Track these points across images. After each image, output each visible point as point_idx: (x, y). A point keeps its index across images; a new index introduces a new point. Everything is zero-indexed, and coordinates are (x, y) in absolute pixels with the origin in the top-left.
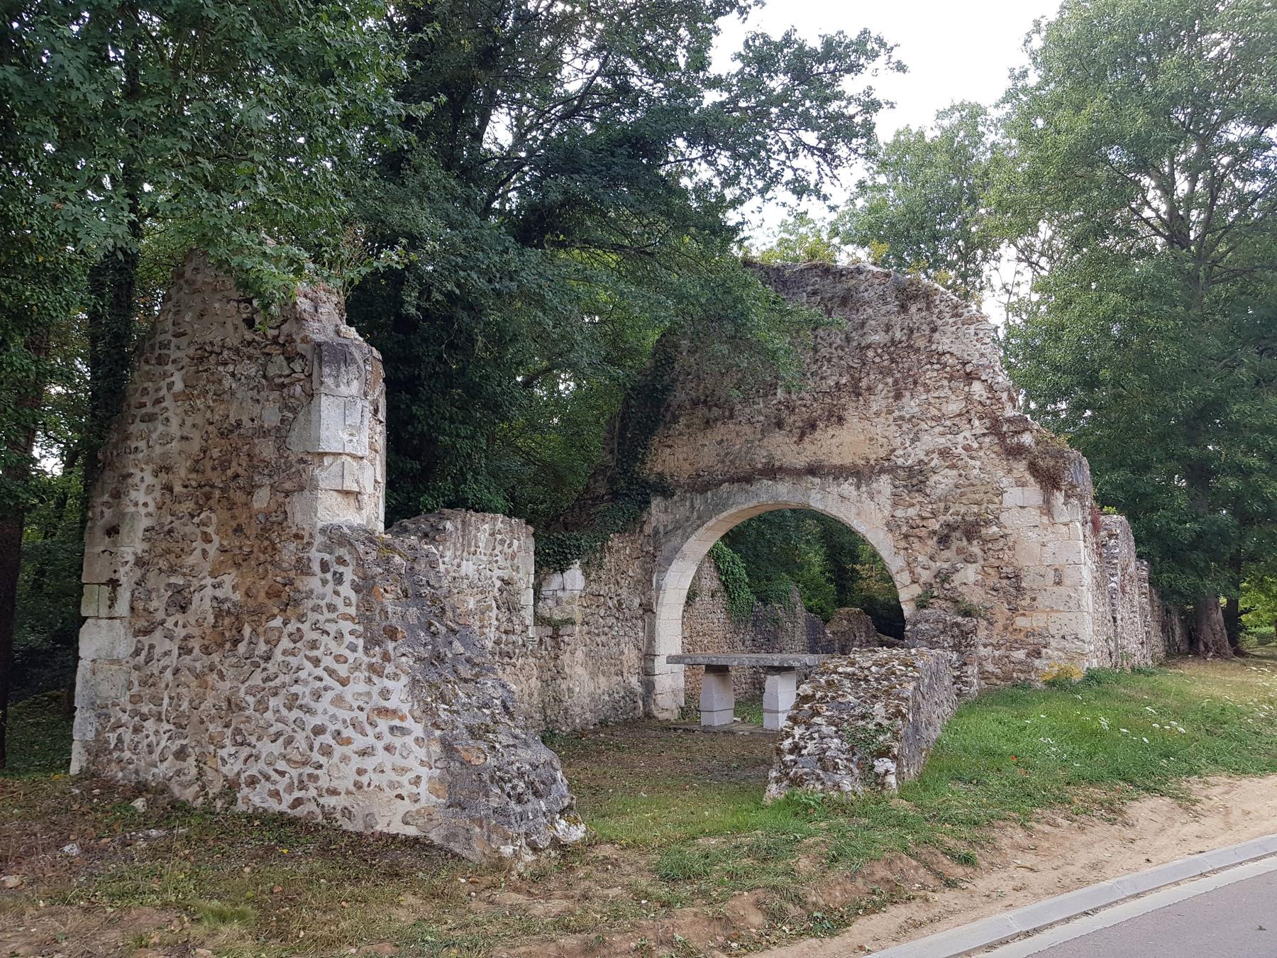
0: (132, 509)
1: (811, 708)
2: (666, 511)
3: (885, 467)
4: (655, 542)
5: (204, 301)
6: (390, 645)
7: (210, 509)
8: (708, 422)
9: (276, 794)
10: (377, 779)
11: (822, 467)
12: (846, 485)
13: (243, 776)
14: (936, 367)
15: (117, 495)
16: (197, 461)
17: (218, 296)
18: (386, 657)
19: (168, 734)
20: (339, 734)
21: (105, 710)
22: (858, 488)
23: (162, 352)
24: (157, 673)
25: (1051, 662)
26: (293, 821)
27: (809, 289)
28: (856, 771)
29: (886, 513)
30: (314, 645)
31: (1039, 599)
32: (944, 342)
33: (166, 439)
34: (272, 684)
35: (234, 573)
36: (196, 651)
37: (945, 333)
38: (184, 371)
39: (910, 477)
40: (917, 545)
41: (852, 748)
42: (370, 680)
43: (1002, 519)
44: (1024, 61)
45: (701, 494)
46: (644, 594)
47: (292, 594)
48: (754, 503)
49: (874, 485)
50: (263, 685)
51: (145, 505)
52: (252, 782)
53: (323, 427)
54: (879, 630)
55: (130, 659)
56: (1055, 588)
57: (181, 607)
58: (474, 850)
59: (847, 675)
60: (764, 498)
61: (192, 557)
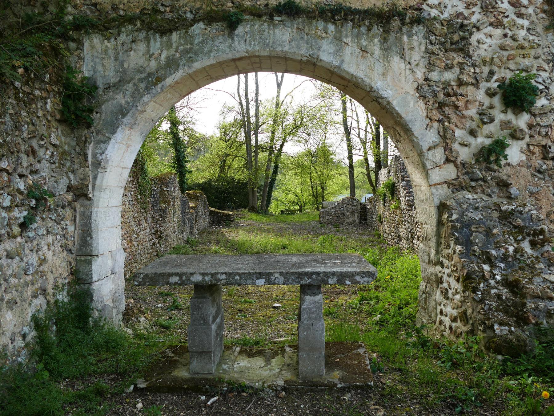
29: (420, 75)
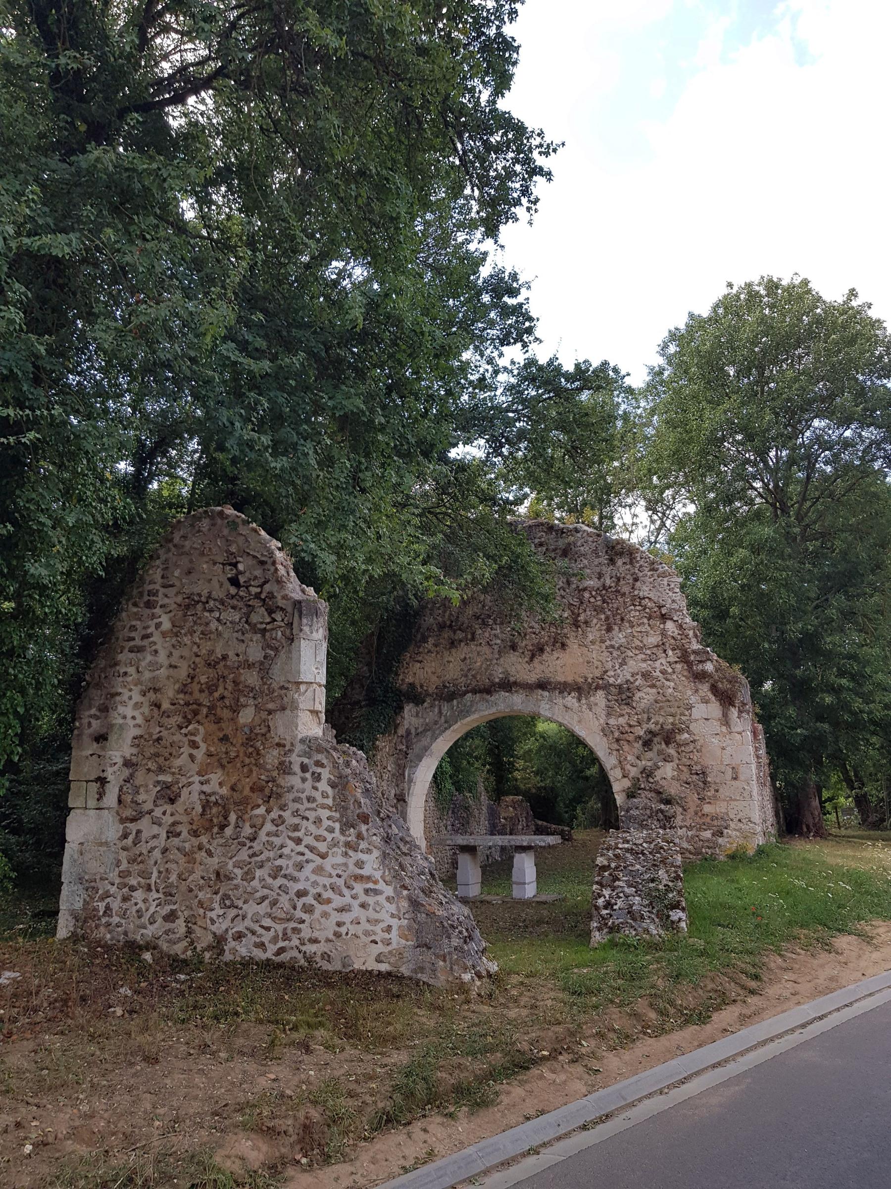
0: (120, 721)
1: (610, 875)
2: (417, 715)
3: (599, 685)
4: (407, 742)
5: (191, 561)
6: (364, 828)
7: (198, 722)
8: (452, 643)
9: (261, 945)
10: (353, 929)
11: (550, 683)
12: (569, 698)
13: (230, 933)
14: (638, 608)
15: (105, 709)
16: (185, 685)
17: (206, 559)
18: (360, 836)
19: (156, 902)
20: (320, 896)
21: (93, 884)
22: (579, 700)
23: (152, 598)
24: (145, 852)
25: (731, 840)
26: (281, 965)
27: (537, 541)
28: (657, 920)
29: (602, 721)
30: (296, 828)
31: (721, 790)
32: (644, 590)
33: (155, 666)
34: (258, 859)
35: (220, 772)
36: (185, 834)
37: (645, 583)
38: (172, 614)
39: (620, 693)
40: (626, 747)
41: (651, 903)
42: (346, 853)
43: (691, 727)
44: (660, 361)
45: (448, 702)
46: (397, 786)
47: (274, 789)
48: (494, 710)
49: (592, 699)
50: (249, 860)
51: (134, 718)
52: (239, 936)
53: (302, 663)
54: (537, 816)
55: (117, 842)
56: (733, 782)
57: (171, 799)
58: (439, 978)
59: (627, 850)
60: (502, 707)
61: (179, 760)
